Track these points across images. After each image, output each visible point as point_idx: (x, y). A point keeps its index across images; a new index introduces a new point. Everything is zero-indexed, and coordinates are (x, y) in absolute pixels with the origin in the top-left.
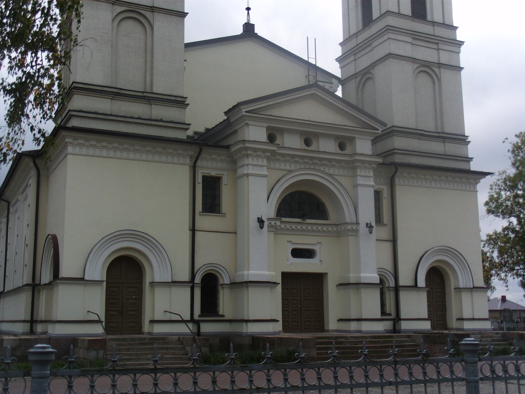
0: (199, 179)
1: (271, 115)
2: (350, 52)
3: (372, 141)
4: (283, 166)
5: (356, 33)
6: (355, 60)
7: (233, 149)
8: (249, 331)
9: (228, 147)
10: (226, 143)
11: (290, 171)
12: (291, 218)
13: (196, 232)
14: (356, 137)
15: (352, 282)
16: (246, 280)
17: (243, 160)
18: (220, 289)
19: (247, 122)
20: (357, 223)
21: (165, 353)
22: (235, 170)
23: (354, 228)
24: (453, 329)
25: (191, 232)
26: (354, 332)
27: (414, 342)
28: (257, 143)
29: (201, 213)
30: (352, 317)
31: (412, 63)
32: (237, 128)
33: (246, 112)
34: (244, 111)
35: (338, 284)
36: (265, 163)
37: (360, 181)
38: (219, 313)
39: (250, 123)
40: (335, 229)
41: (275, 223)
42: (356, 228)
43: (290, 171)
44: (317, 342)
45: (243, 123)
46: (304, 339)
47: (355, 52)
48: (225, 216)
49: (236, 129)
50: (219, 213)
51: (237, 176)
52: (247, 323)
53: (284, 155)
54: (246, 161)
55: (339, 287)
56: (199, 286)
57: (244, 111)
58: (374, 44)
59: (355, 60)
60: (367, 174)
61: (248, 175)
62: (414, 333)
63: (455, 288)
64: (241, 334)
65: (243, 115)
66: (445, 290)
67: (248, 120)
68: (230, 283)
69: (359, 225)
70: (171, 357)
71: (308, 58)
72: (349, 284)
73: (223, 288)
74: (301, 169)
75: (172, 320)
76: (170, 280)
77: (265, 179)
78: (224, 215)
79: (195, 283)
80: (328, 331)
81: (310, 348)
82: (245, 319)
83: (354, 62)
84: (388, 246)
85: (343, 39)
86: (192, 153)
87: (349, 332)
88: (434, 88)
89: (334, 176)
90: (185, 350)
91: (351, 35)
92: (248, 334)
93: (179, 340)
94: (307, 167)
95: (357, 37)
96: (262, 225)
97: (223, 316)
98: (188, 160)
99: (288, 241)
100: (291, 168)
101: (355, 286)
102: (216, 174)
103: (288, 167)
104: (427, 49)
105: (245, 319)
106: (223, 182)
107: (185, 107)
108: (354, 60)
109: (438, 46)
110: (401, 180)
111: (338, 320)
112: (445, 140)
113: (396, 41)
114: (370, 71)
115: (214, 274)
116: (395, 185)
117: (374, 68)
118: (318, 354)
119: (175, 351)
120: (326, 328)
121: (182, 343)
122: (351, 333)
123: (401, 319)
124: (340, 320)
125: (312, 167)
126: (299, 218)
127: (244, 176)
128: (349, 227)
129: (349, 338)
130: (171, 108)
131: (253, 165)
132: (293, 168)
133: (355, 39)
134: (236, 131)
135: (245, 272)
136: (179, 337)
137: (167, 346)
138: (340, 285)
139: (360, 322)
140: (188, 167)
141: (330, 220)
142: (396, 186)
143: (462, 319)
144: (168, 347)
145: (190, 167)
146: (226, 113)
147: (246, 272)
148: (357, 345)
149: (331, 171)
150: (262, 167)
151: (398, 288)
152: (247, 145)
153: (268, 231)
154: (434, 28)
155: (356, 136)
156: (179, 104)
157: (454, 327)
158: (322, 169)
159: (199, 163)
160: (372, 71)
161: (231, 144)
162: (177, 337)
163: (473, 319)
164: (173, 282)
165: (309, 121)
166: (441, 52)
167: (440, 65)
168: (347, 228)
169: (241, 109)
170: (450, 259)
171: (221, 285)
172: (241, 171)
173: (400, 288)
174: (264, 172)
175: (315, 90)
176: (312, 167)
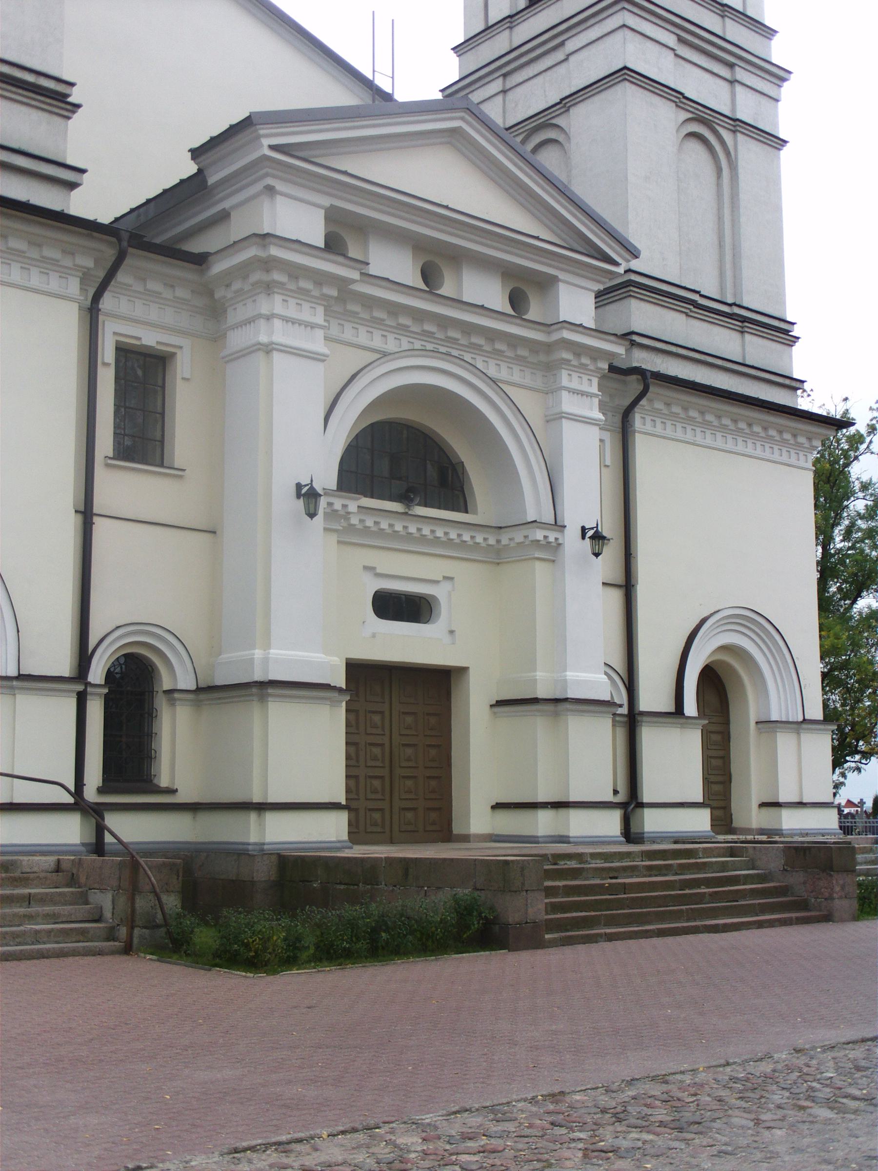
0: (108, 353)
1: (345, 173)
2: (493, 66)
3: (599, 295)
4: (363, 338)
5: (509, 17)
6: (504, 92)
7: (218, 267)
8: (268, 839)
9: (200, 260)
10: (196, 246)
11: (385, 354)
12: (372, 497)
13: (96, 519)
14: (560, 277)
15: (541, 695)
16: (258, 676)
17: (254, 301)
18: (162, 705)
19: (270, 181)
20: (558, 526)
21: (25, 916)
22: (217, 338)
23: (551, 539)
24: (748, 831)
25: (80, 517)
26: (547, 839)
27: (753, 869)
28: (304, 249)
29: (110, 462)
30: (541, 799)
31: (673, 105)
32: (226, 204)
33: (272, 147)
34: (266, 142)
35: (494, 702)
36: (319, 318)
37: (569, 404)
38: (155, 781)
39: (279, 186)
40: (492, 541)
41: (345, 506)
42: (556, 539)
43: (385, 354)
44: (545, 870)
45: (259, 187)
46: (512, 861)
47: (508, 69)
48: (181, 477)
49: (224, 209)
50: (162, 465)
51: (226, 352)
52: (259, 815)
53: (370, 302)
54: (264, 306)
55: (498, 709)
56: (99, 695)
57: (266, 142)
58: (570, 46)
59: (504, 92)
60: (585, 387)
61: (268, 349)
62: (676, 842)
63: (757, 723)
64: (241, 847)
65: (265, 158)
66: (729, 728)
67: (274, 177)
68: (194, 687)
69: (562, 532)
70: (50, 932)
71: (374, 71)
72: (535, 701)
73: (172, 703)
74: (411, 352)
75: (16, 801)
76: (12, 672)
77: (321, 365)
78: (178, 474)
79: (90, 683)
80: (465, 838)
81: (527, 891)
82: (254, 801)
83: (500, 98)
84: (616, 597)
85: (465, 35)
86: (89, 263)
87: (532, 840)
88: (719, 185)
89: (504, 387)
90: (87, 903)
91: (490, 24)
92: (266, 847)
93: (58, 869)
94: (430, 347)
95: (511, 28)
96: (312, 506)
97: (172, 791)
98: (73, 286)
99: (366, 568)
100: (384, 346)
101: (550, 707)
102: (157, 342)
103: (377, 342)
104: (707, 76)
105: (256, 799)
106: (179, 371)
107: (66, 113)
108: (502, 91)
109: (733, 73)
110: (648, 419)
111: (493, 807)
112: (747, 324)
113: (638, 36)
114: (554, 121)
115: (147, 657)
116: (634, 431)
117: (568, 110)
118: (555, 908)
119: (57, 909)
120: (457, 829)
121: (72, 881)
122: (538, 843)
123: (641, 805)
124: (498, 806)
125: (443, 349)
126: (391, 499)
127: (259, 349)
128: (539, 535)
129: (589, 859)
130: (24, 109)
131: (286, 320)
132: (391, 345)
133: (507, 32)
134: (224, 216)
135: (257, 651)
136: (59, 861)
137: (27, 891)
138: (500, 703)
139: (562, 812)
140: (75, 307)
141: (475, 512)
142: (637, 434)
143: (777, 805)
144: (30, 894)
145: (80, 308)
146: (196, 153)
147: (258, 653)
148: (616, 878)
149: (492, 372)
150: (312, 327)
151: (639, 718)
152: (275, 251)
153: (325, 529)
154: (724, 22)
155: (561, 275)
156: (48, 101)
157: (755, 825)
158: (467, 357)
159: (107, 302)
160: (560, 121)
161: (212, 250)
162: (52, 859)
163: (801, 804)
164: (21, 677)
165: (447, 207)
166: (739, 88)
167: (737, 125)
168: (531, 538)
169: (259, 137)
170: (752, 644)
171: (167, 692)
172: (237, 339)
173: (645, 719)
174: (316, 343)
175: (462, 119)
176: (443, 349)
